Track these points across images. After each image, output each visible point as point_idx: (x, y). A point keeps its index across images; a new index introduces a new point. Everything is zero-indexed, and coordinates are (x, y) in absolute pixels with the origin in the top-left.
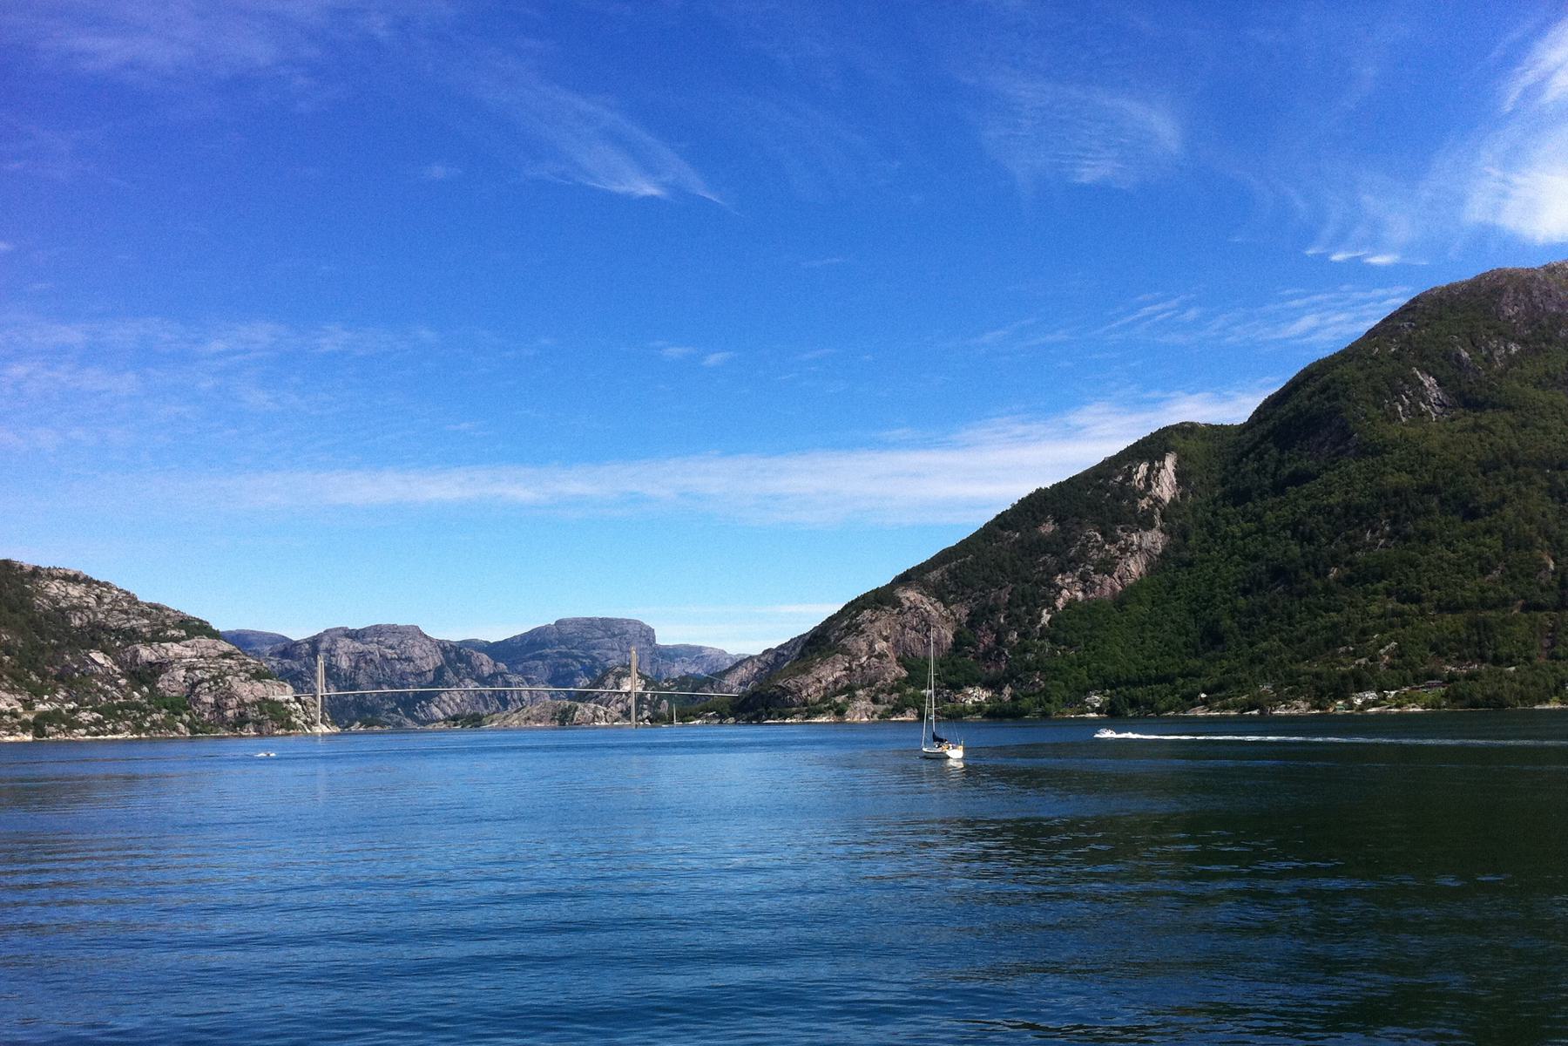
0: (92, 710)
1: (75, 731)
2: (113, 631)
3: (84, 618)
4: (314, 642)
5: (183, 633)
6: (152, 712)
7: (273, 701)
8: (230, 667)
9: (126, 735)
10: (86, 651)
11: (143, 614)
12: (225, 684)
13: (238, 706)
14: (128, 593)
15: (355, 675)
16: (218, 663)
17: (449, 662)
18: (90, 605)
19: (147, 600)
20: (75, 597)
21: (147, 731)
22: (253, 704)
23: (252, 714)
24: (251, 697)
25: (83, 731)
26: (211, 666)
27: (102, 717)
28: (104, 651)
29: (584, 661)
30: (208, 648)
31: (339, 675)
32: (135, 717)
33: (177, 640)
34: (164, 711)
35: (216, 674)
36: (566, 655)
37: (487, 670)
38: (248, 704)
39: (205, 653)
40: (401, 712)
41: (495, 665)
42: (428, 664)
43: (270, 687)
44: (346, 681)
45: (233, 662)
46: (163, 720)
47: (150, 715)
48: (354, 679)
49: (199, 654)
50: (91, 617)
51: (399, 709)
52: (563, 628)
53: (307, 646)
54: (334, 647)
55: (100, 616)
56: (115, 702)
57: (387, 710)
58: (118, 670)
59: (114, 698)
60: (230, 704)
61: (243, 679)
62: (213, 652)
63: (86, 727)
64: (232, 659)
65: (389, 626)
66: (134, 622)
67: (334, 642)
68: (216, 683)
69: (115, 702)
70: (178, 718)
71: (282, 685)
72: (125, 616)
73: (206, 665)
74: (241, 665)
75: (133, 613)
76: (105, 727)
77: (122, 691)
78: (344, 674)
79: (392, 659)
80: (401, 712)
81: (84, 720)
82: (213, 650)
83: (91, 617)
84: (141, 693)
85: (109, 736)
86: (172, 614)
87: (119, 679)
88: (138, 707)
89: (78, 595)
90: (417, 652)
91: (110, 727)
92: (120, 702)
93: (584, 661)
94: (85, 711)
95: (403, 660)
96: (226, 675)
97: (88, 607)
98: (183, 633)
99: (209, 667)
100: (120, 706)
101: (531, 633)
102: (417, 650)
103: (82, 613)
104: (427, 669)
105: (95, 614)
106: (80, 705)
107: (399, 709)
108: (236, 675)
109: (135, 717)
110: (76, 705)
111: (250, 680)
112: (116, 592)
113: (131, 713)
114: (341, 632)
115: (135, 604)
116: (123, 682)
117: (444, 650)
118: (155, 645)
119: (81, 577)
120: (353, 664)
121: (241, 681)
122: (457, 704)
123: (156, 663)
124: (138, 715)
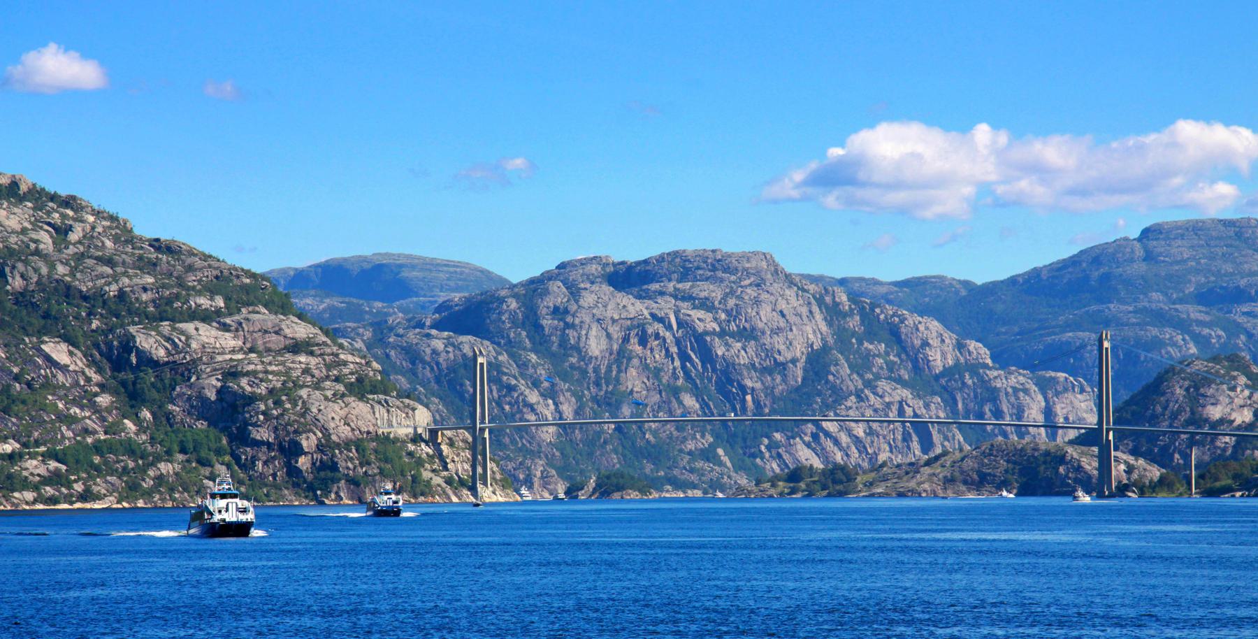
0: (47, 456)
1: (16, 494)
2: (85, 298)
3: (31, 273)
4: (536, 287)
5: (220, 302)
6: (158, 459)
7: (386, 438)
8: (306, 371)
9: (109, 502)
10: (35, 339)
11: (147, 266)
12: (294, 403)
13: (320, 448)
14: (113, 218)
15: (619, 371)
16: (283, 363)
17: (843, 337)
18: (42, 246)
19: (149, 234)
20: (13, 232)
21: (148, 494)
22: (347, 444)
23: (347, 463)
24: (345, 432)
25: (29, 496)
26: (270, 368)
27: (64, 468)
28: (69, 340)
29: (1206, 331)
30: (266, 332)
31: (584, 372)
32: (125, 468)
33: (206, 317)
34: (180, 457)
35: (279, 385)
36: (1160, 318)
37: (941, 355)
38: (338, 445)
39: (260, 342)
40: (726, 459)
41: (960, 346)
42: (790, 344)
43: (383, 411)
44: (597, 384)
45: (313, 361)
46: (176, 474)
47: (153, 464)
48: (617, 380)
49: (248, 345)
50: (44, 271)
51: (720, 451)
52: (1157, 245)
53: (513, 304)
54: (573, 307)
55: (61, 269)
56: (89, 440)
57: (690, 453)
58: (96, 378)
59: (86, 431)
60: (304, 444)
61: (329, 394)
62: (275, 341)
63: (36, 488)
64: (312, 353)
65: (702, 256)
66: (126, 281)
67: (574, 291)
68: (278, 403)
69: (89, 440)
70: (206, 471)
71: (408, 406)
72: (108, 270)
73: (260, 367)
74: (329, 367)
75: (124, 263)
76: (69, 487)
77: (103, 419)
78: (596, 370)
79: (706, 333)
80: (726, 459)
81: (32, 474)
82: (274, 337)
83: (44, 271)
84: (138, 421)
85: (78, 505)
86: (198, 263)
87: (96, 395)
88: (131, 450)
89: (18, 227)
90: (765, 317)
91: (79, 487)
92: (99, 441)
93: (1206, 331)
94: (33, 456)
95: (732, 335)
96: (297, 386)
97: (37, 252)
98: (220, 302)
99: (266, 372)
100: (98, 448)
101: (1074, 261)
102: (766, 312)
103: (26, 263)
104: (789, 356)
105: (52, 267)
106: (25, 445)
107: (720, 451)
108: (317, 386)
109: (125, 468)
110: (18, 446)
111: (343, 395)
112: (91, 219)
113: (118, 462)
114: (594, 269)
115: (127, 242)
116: (104, 400)
117: (833, 313)
118: (165, 326)
119: (23, 188)
120: (615, 347)
121: (326, 399)
122: (857, 440)
123: (168, 363)
124: (131, 464)
